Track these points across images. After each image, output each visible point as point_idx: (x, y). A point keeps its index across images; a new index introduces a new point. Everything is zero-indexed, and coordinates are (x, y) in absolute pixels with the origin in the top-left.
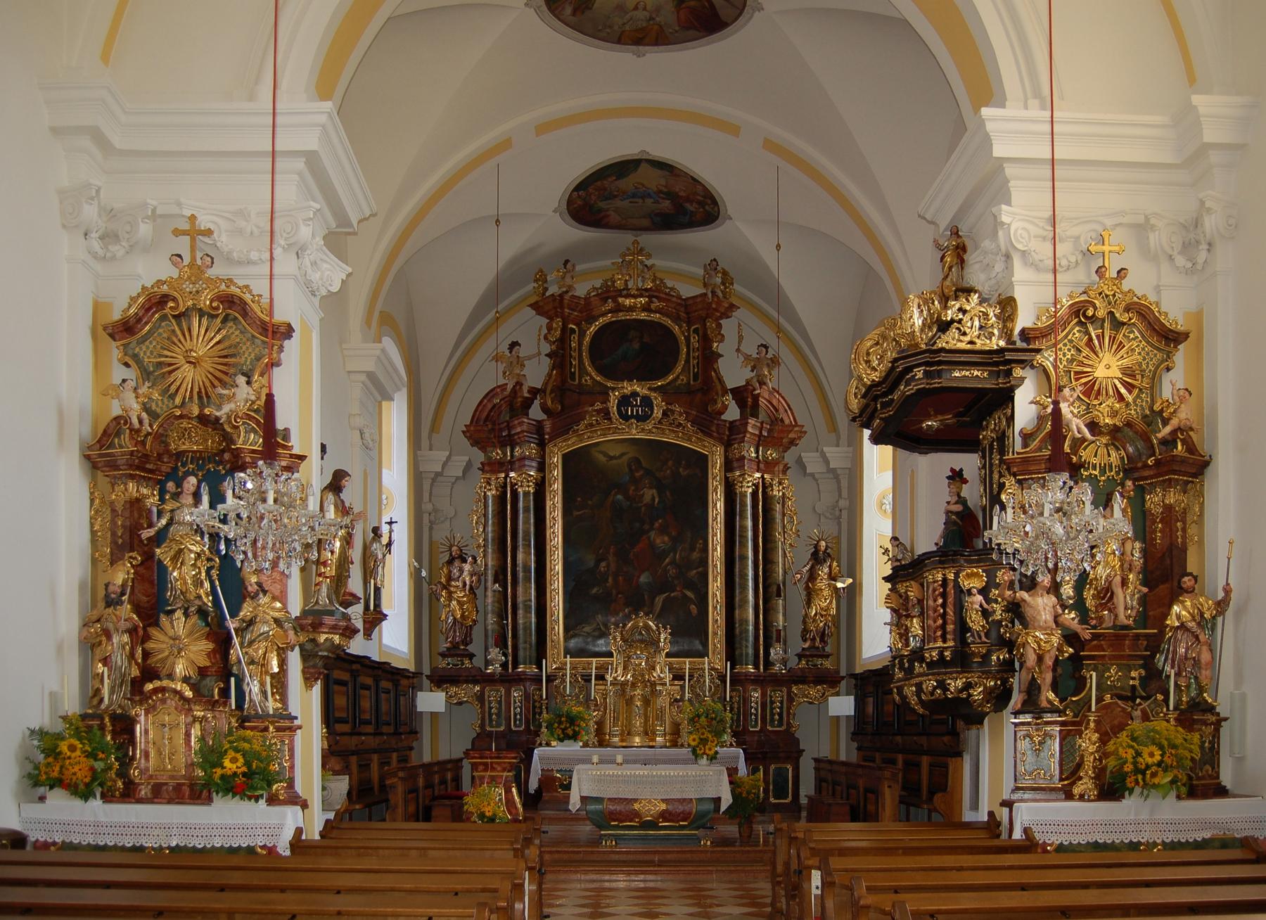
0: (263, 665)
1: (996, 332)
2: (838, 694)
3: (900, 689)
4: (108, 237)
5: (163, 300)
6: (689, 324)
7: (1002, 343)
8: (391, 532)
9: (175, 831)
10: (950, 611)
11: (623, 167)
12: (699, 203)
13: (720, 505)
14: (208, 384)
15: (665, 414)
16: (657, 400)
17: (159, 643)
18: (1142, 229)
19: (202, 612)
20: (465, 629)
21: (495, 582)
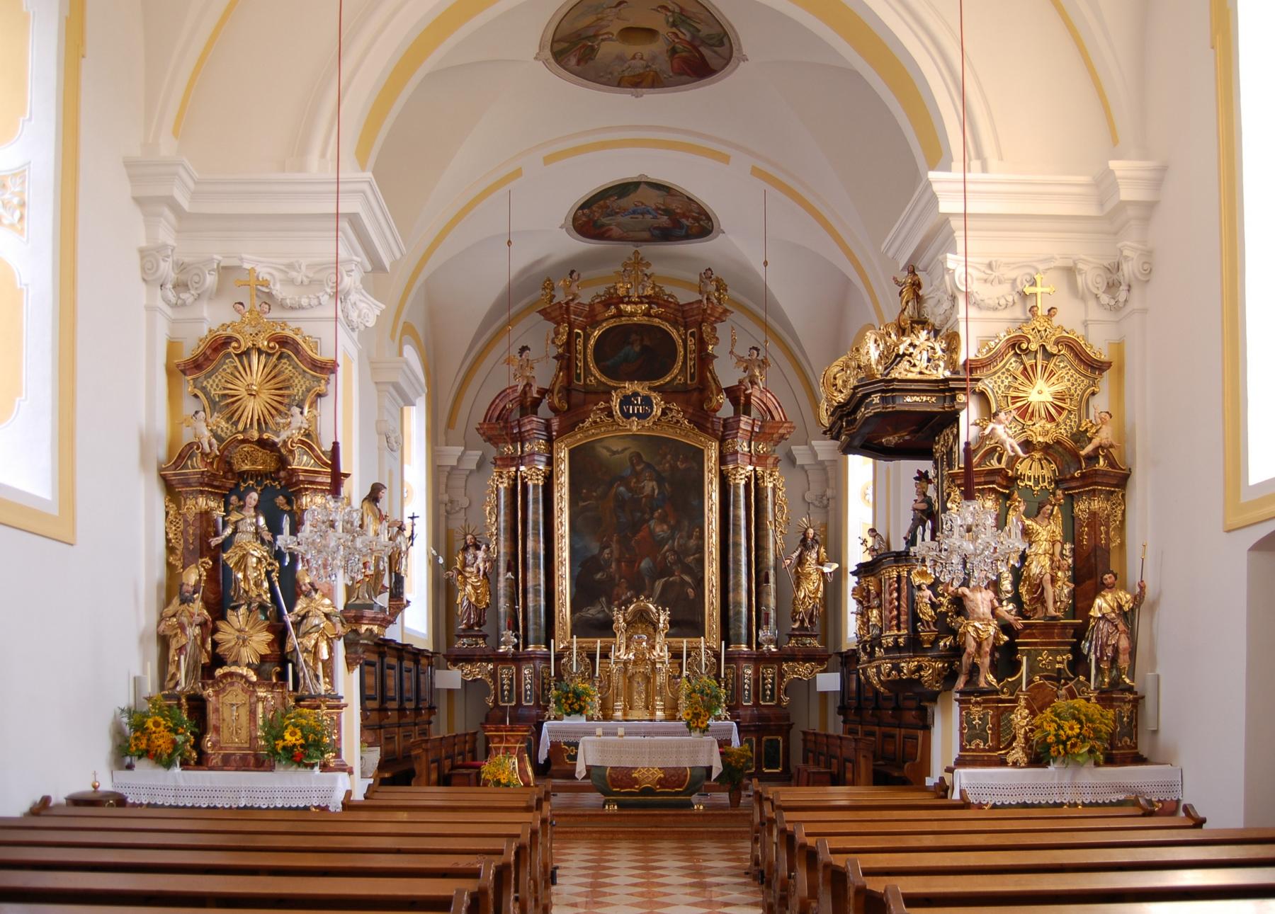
0: (315, 652)
1: (942, 364)
2: (825, 671)
3: (864, 670)
4: (180, 286)
5: (227, 341)
6: (686, 329)
7: (948, 374)
8: (413, 525)
9: (243, 794)
10: (903, 604)
11: (624, 189)
12: (694, 218)
13: (716, 496)
14: (266, 412)
15: (664, 413)
16: (656, 398)
17: (227, 634)
18: (1070, 272)
19: (262, 607)
20: (481, 616)
21: (508, 570)
